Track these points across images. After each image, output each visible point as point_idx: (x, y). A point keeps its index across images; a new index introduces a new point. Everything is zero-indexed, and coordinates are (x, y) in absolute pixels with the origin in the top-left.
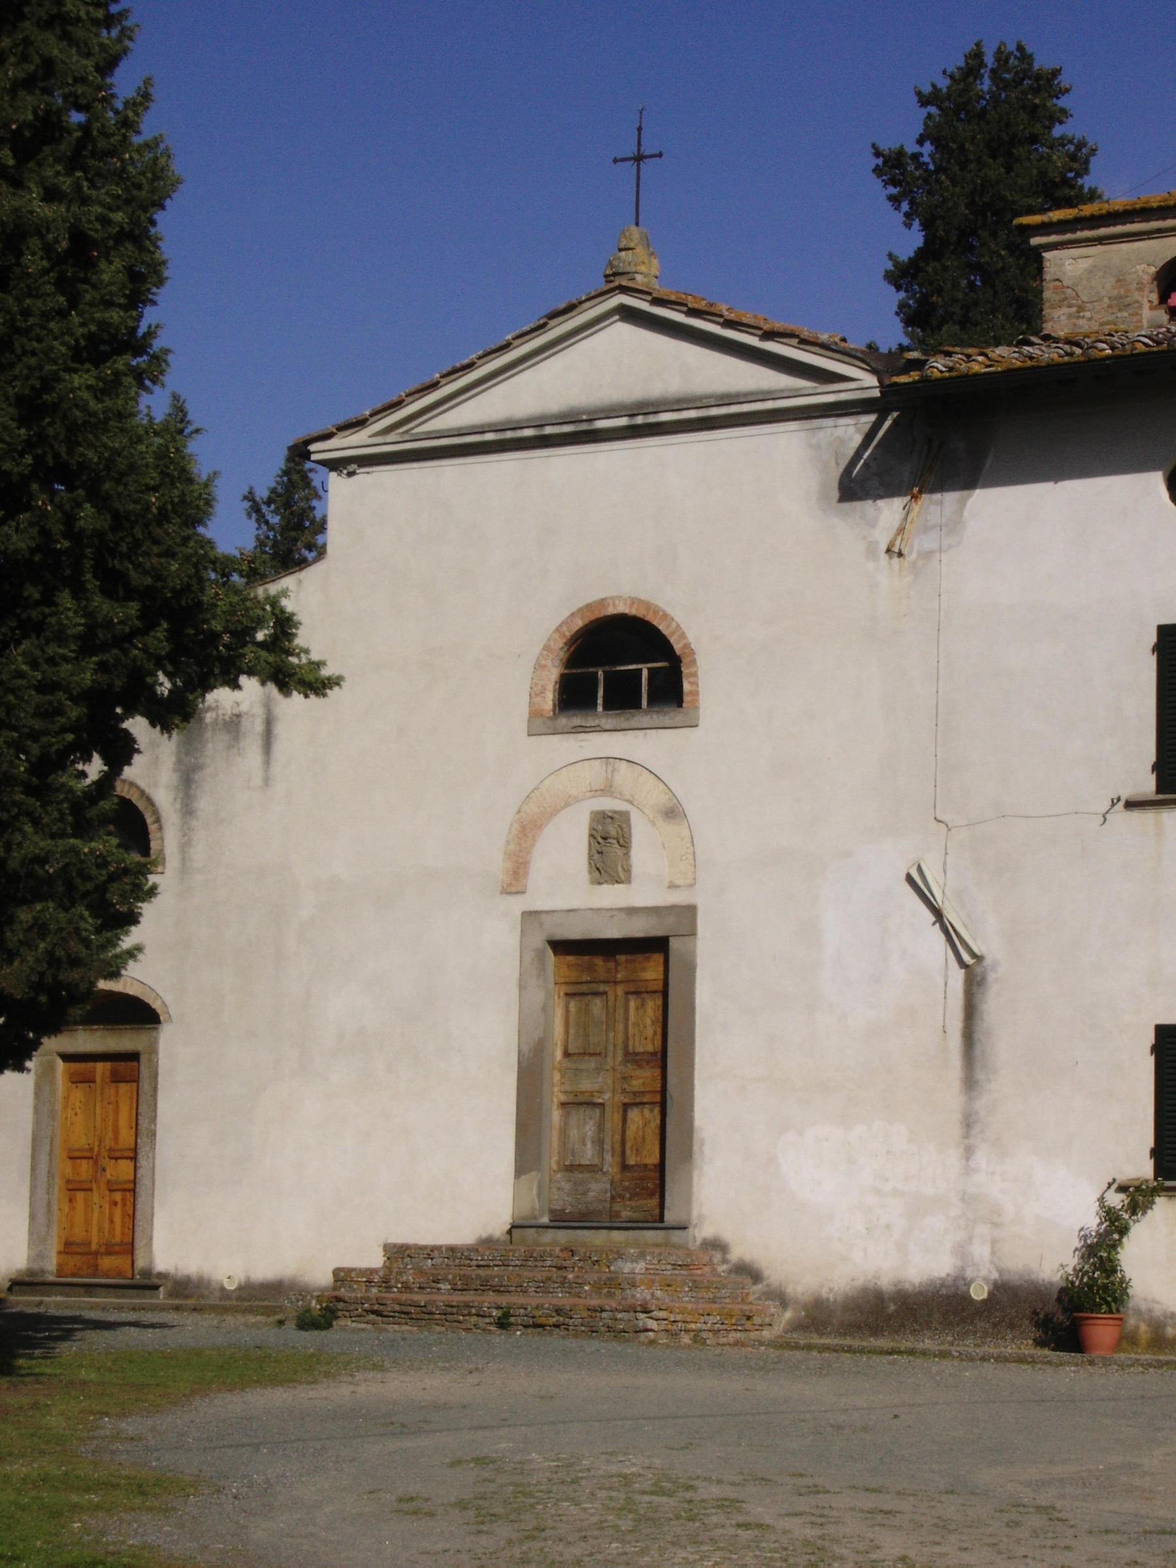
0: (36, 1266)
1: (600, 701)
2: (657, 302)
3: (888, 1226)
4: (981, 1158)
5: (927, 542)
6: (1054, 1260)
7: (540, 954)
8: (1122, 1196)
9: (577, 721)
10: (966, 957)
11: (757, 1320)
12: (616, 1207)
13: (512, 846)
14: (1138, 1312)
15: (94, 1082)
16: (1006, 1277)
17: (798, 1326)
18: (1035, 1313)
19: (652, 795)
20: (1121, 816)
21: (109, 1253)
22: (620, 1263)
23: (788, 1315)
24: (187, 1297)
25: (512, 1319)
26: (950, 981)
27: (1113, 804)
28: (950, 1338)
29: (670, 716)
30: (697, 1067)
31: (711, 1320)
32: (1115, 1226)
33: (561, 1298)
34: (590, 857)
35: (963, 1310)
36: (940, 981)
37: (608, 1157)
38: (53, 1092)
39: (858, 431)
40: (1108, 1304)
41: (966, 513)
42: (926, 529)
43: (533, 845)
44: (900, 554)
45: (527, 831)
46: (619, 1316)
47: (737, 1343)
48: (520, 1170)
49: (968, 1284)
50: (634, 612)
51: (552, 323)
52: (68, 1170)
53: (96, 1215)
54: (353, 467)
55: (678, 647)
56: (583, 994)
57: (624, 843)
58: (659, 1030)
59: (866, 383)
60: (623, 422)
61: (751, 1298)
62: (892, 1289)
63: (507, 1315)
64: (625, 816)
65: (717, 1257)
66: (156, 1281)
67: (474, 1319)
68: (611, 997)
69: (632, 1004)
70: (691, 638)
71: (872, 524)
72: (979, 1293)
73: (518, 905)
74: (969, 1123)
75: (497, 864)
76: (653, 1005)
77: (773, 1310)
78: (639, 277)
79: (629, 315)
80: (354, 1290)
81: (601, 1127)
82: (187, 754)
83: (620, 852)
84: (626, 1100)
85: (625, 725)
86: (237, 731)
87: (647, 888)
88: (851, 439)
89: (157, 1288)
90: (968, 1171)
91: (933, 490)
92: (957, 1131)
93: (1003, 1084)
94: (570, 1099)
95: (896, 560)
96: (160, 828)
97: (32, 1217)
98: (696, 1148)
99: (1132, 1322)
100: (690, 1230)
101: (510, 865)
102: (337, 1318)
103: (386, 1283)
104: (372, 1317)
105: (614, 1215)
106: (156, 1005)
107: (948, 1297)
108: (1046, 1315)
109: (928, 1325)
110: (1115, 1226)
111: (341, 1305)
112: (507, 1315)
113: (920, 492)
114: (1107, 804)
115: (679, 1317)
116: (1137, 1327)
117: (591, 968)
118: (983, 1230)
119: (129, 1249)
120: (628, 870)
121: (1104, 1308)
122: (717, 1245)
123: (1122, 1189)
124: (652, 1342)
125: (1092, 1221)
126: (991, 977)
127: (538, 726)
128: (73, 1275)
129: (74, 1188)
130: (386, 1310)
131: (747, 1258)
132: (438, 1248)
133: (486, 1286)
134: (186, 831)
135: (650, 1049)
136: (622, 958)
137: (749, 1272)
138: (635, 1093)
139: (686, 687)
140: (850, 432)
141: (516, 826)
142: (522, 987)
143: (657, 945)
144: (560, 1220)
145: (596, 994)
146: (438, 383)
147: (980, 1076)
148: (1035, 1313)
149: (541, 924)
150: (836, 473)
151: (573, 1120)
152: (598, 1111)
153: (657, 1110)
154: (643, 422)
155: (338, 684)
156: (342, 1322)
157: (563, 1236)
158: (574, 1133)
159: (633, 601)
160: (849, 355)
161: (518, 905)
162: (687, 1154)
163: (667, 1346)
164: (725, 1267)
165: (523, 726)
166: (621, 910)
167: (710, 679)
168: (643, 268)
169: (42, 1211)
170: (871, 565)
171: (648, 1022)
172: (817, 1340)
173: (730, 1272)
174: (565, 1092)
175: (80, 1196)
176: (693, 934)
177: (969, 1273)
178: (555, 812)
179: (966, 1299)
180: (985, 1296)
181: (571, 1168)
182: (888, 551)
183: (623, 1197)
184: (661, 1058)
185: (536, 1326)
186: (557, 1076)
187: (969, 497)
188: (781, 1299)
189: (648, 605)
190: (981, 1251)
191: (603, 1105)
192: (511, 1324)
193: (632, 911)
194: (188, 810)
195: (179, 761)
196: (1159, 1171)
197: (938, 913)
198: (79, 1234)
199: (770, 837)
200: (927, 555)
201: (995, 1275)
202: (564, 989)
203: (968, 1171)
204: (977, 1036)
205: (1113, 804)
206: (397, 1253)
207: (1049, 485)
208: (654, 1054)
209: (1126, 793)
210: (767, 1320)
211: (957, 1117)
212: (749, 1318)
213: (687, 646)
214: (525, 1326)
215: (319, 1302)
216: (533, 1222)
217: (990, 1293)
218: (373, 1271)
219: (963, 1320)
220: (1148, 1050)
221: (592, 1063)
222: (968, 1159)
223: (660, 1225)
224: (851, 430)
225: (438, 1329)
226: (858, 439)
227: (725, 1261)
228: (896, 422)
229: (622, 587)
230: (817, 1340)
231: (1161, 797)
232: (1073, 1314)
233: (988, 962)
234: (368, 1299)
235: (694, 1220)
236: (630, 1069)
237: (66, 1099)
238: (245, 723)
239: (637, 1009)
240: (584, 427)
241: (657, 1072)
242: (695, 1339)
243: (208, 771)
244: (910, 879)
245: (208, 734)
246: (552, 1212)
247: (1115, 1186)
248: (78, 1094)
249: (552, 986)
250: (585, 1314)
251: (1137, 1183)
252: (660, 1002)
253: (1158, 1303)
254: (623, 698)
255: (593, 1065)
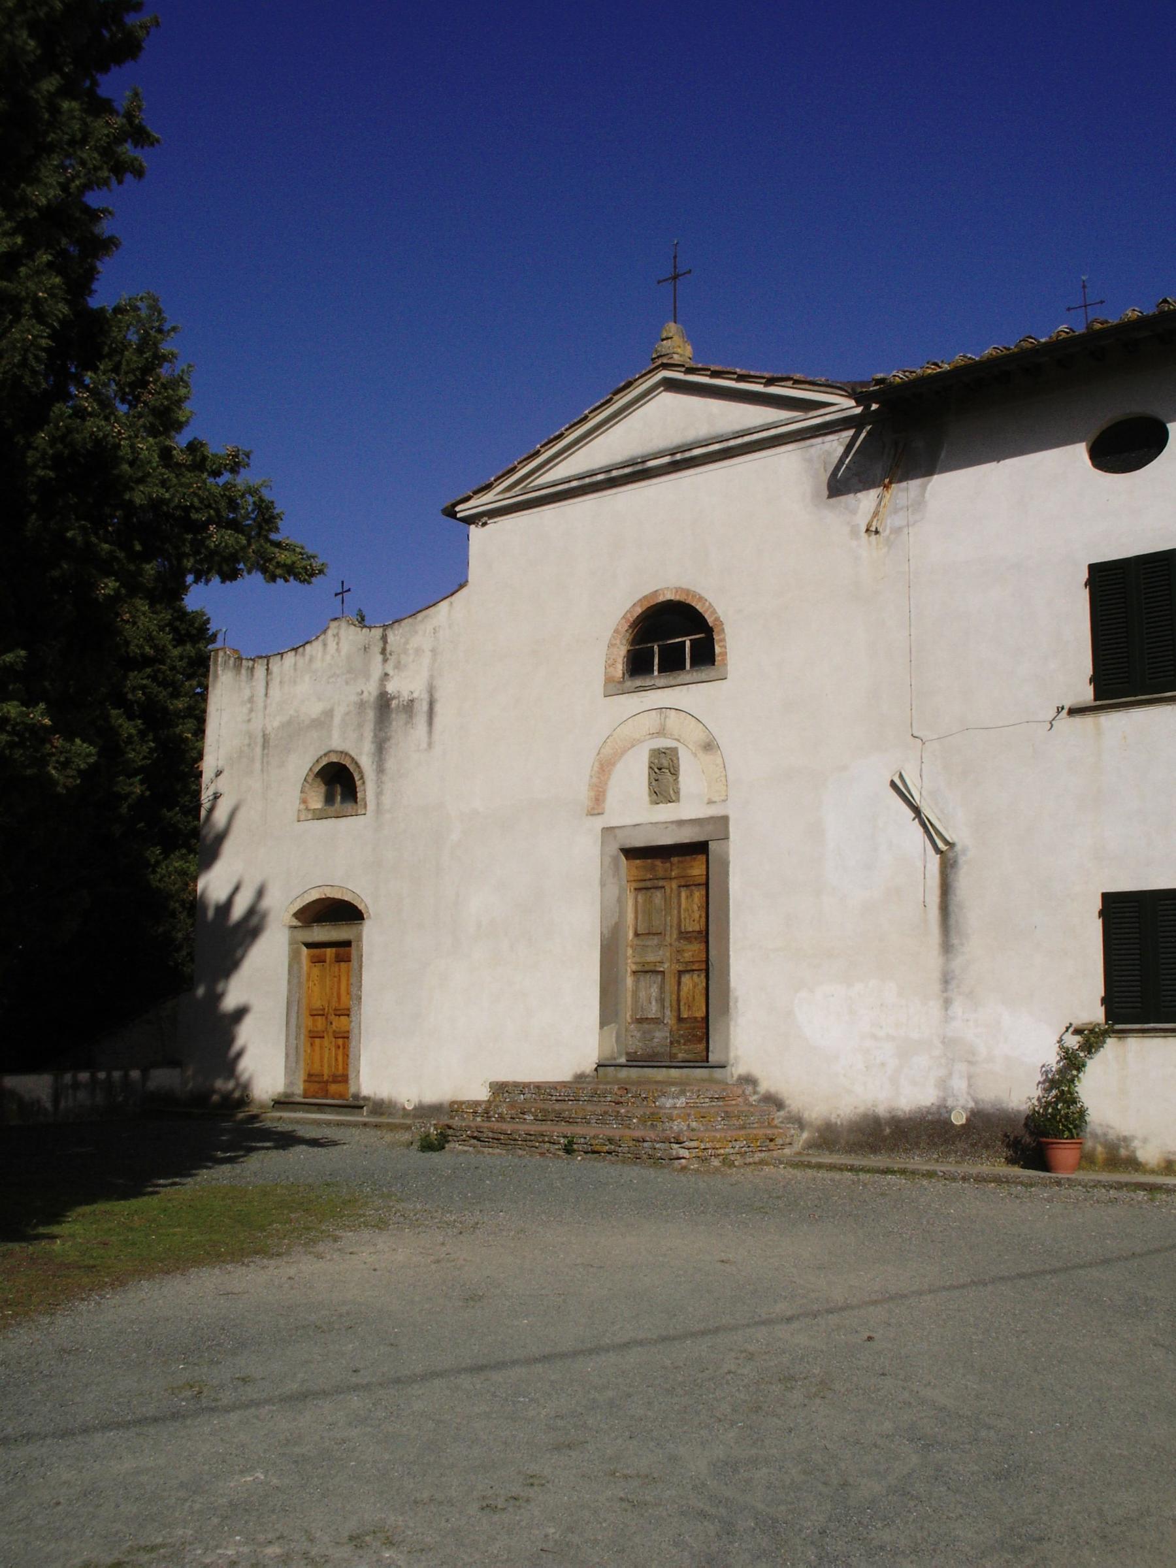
0: (289, 1091)
1: (656, 668)
2: (690, 371)
3: (883, 1064)
4: (957, 1008)
5: (898, 520)
6: (1021, 1093)
7: (615, 859)
8: (1078, 1038)
9: (639, 682)
10: (941, 845)
11: (779, 1141)
12: (674, 1051)
13: (595, 780)
14: (1095, 1136)
15: (324, 961)
16: (981, 1106)
17: (811, 1145)
18: (1006, 1136)
19: (694, 734)
20: (1067, 724)
21: (334, 1082)
22: (663, 1099)
23: (805, 1135)
24: (382, 1114)
25: (575, 1147)
26: (928, 865)
27: (1059, 712)
28: (935, 1156)
29: (705, 673)
30: (731, 940)
31: (738, 1145)
32: (1072, 1063)
33: (614, 1130)
34: (650, 784)
35: (946, 1132)
36: (920, 865)
37: (668, 1012)
38: (300, 968)
39: (841, 444)
40: (1070, 1130)
41: (927, 495)
42: (896, 511)
43: (609, 778)
44: (877, 532)
45: (605, 767)
46: (657, 1146)
47: (762, 1162)
48: (603, 1024)
49: (949, 1112)
50: (678, 598)
51: (616, 398)
52: (310, 1023)
53: (326, 1055)
54: (485, 519)
55: (710, 621)
56: (647, 889)
57: (675, 772)
58: (704, 915)
59: (846, 405)
60: (667, 459)
61: (776, 1122)
62: (888, 1115)
63: (571, 1143)
64: (674, 751)
65: (749, 1089)
66: (362, 1103)
67: (547, 1145)
68: (668, 890)
69: (683, 895)
70: (720, 613)
71: (854, 512)
72: (959, 1119)
73: (599, 823)
74: (946, 980)
75: (583, 794)
76: (698, 894)
77: (793, 1132)
78: (675, 356)
79: (672, 385)
80: (464, 1119)
81: (662, 989)
82: (380, 730)
83: (671, 778)
84: (681, 968)
85: (673, 683)
86: (412, 711)
87: (691, 805)
88: (835, 450)
89: (362, 1107)
90: (947, 1019)
91: (900, 481)
92: (936, 987)
93: (975, 944)
94: (639, 968)
95: (873, 537)
96: (364, 783)
97: (287, 1055)
98: (731, 1004)
99: (1089, 1144)
100: (729, 1068)
101: (593, 794)
102: (448, 1142)
103: (487, 1115)
104: (475, 1141)
105: (673, 1057)
106: (361, 907)
107: (932, 1122)
108: (1016, 1138)
109: (917, 1144)
110: (1072, 1063)
111: (450, 1132)
112: (571, 1143)
113: (891, 483)
114: (1053, 712)
115: (708, 1145)
116: (1094, 1149)
117: (653, 868)
118: (961, 1067)
119: (344, 1079)
120: (677, 793)
121: (1067, 1134)
122: (749, 1080)
123: (1078, 1032)
124: (684, 1169)
125: (1052, 1058)
126: (962, 860)
127: (613, 689)
128: (314, 1097)
129: (314, 1036)
130: (483, 1136)
131: (773, 1090)
132: (526, 1085)
133: (560, 1118)
134: (379, 783)
135: (697, 928)
136: (675, 860)
137: (774, 1101)
138: (687, 963)
139: (717, 650)
140: (834, 445)
141: (597, 764)
142: (603, 885)
143: (700, 848)
144: (634, 1061)
145: (657, 888)
146: (539, 451)
147: (955, 941)
148: (1006, 1136)
149: (615, 837)
150: (825, 477)
151: (642, 984)
152: (659, 978)
153: (703, 975)
154: (681, 460)
155: (321, 572)
156: (452, 1145)
157: (634, 1073)
158: (642, 994)
159: (677, 590)
160: (829, 386)
161: (599, 823)
162: (725, 1009)
163: (697, 1171)
164: (755, 1097)
165: (600, 690)
166: (672, 822)
167: (734, 644)
168: (679, 350)
169: (292, 1052)
170: (854, 543)
171: (695, 908)
172: (828, 1159)
173: (760, 1101)
174: (635, 963)
175: (317, 1041)
176: (727, 838)
177: (950, 1103)
178: (625, 751)
179: (947, 1123)
180: (964, 1121)
181: (640, 1021)
182: (867, 530)
183: (678, 1042)
184: (704, 936)
185: (594, 1152)
186: (630, 951)
187: (929, 482)
188: (799, 1122)
189: (687, 592)
190: (959, 1085)
191: (663, 972)
192: (574, 1151)
193: (681, 823)
194: (380, 770)
195: (375, 736)
196: (1109, 1016)
197: (917, 811)
198: (316, 1068)
199: (794, 774)
200: (898, 531)
201: (971, 1105)
202: (635, 885)
203: (947, 1019)
204: (953, 908)
205: (1059, 712)
206: (499, 1089)
207: (993, 465)
208: (700, 932)
209: (1068, 704)
210: (788, 1140)
211: (936, 975)
212: (771, 1140)
213: (717, 619)
214: (586, 1153)
215: (436, 1129)
216: (613, 1062)
217: (967, 1119)
218: (477, 1103)
219: (946, 1141)
220: (1097, 914)
221: (655, 941)
222: (946, 1009)
223: (706, 1064)
224: (835, 443)
225: (520, 1152)
226: (840, 450)
227: (755, 1093)
228: (869, 433)
229: (668, 580)
230: (828, 1159)
231: (1098, 703)
232: (1041, 1137)
233: (958, 848)
234: (470, 1127)
235: (732, 1061)
236: (683, 944)
237: (309, 975)
238: (416, 705)
239: (687, 897)
240: (639, 467)
241: (703, 946)
242: (724, 1162)
243: (393, 741)
244: (893, 784)
245: (394, 716)
246: (628, 1054)
247: (1071, 1030)
248: (316, 971)
249: (624, 882)
250: (631, 1143)
251: (1090, 1027)
252: (704, 892)
253: (1112, 1128)
254: (672, 663)
255: (655, 942)
